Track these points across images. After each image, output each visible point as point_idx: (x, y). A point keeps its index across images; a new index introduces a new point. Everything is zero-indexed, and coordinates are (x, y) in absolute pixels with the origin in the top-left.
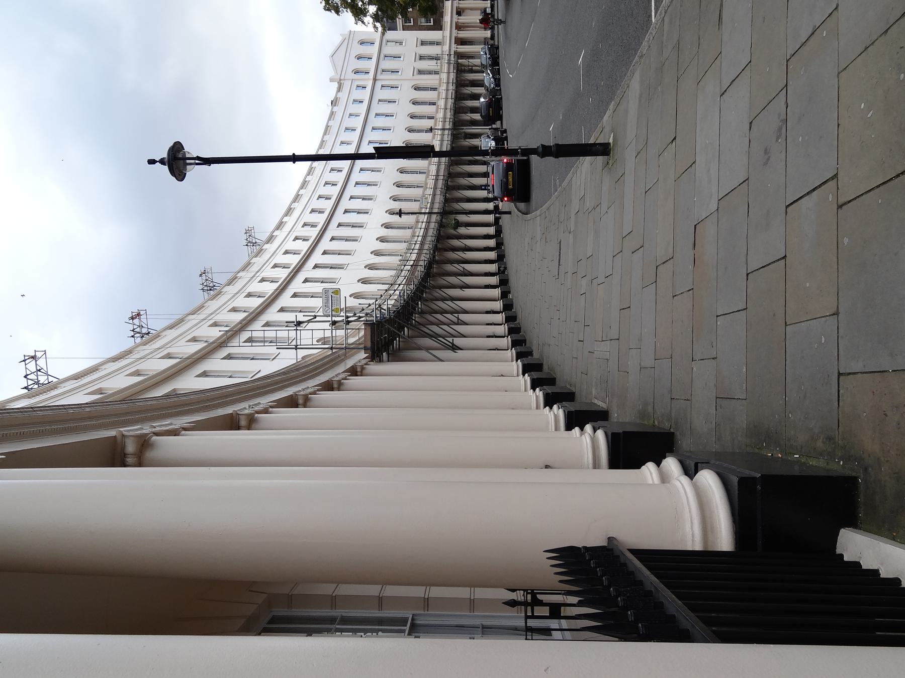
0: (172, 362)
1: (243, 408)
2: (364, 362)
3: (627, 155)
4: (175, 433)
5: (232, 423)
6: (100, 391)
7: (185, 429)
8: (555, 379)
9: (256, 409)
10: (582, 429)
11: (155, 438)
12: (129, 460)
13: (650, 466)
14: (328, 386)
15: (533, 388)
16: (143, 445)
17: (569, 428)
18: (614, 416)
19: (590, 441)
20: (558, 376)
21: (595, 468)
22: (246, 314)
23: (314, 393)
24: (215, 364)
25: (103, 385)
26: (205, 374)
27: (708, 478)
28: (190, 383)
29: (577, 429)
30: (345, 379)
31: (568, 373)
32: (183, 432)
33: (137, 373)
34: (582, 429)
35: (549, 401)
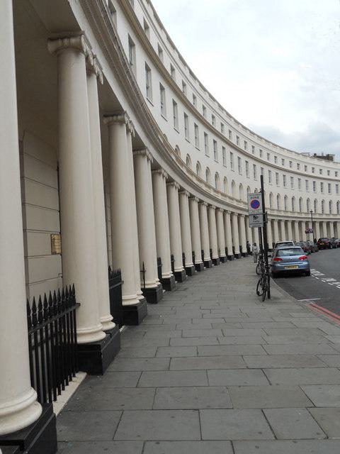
0: (191, 100)
2: (177, 185)
4: (90, 71)
6: (147, 27)
13: (112, 318)
16: (77, 48)
17: (142, 289)
29: (112, 318)
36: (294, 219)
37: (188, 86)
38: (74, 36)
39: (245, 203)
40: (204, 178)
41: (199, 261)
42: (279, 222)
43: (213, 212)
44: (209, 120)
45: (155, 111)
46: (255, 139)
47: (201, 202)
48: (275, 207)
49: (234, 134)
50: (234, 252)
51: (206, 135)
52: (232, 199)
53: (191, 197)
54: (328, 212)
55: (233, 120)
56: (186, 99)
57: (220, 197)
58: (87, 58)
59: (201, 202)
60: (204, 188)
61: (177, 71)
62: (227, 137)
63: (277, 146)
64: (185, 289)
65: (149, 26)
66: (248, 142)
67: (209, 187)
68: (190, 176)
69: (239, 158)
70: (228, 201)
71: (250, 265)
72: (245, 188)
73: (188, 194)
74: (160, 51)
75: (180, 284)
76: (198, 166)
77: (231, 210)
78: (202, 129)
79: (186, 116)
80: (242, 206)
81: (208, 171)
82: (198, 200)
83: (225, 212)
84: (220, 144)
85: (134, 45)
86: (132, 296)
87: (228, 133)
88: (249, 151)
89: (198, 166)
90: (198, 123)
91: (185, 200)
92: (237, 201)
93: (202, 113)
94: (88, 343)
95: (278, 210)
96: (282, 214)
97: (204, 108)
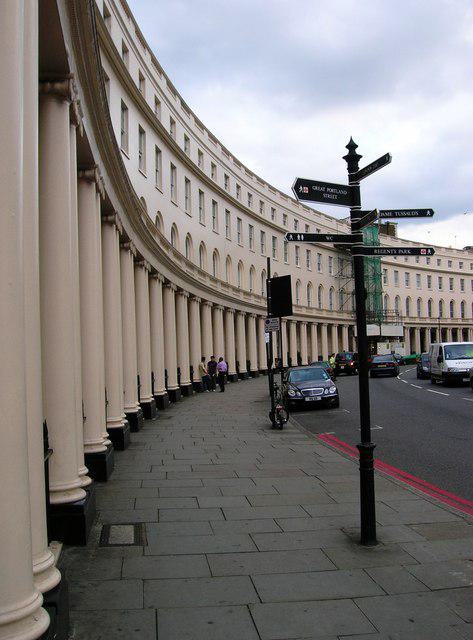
1: (102, 173)
2: (148, 267)
3: (275, 437)
4: (73, 120)
5: (85, 164)
6: (107, 15)
7: (78, 129)
8: (123, 450)
9: (100, 183)
10: (108, 438)
11: (68, 104)
12: (105, 218)
13: (87, 471)
14: (124, 240)
15: (141, 405)
16: (62, 95)
17: (108, 430)
18: (118, 455)
19: (101, 442)
20: (126, 453)
21: (85, 446)
22: (183, 148)
23: (98, 190)
24: (135, 120)
25: (114, 20)
26: (124, 108)
27: (83, 494)
28: (115, 96)
29: (87, 471)
30: (131, 253)
31: (125, 466)
32: (74, 127)
33: (125, 51)
34: (108, 438)
35: (130, 417)
36: (341, 323)
37: (192, 141)
38: (61, 80)
39: (258, 297)
40: (182, 250)
41: (186, 381)
42: (309, 325)
43: (208, 311)
44: (194, 158)
45: (131, 165)
46: (265, 191)
47: (191, 297)
48: (314, 304)
49: (221, 171)
50: (237, 369)
51: (187, 181)
52: (237, 290)
53: (179, 292)
54: (404, 314)
55: (232, 160)
56: (159, 123)
57: (219, 289)
58: (72, 107)
59: (191, 297)
60: (185, 268)
61: (147, 81)
62: (234, 196)
63: (320, 214)
64: (169, 418)
65: (111, 13)
66: (232, 178)
67: (203, 274)
68: (178, 262)
69: (251, 227)
70: (230, 293)
71: (262, 386)
72: (235, 262)
73: (148, 267)
74: (125, 51)
75: (160, 413)
76: (174, 230)
77: (234, 306)
78: (196, 185)
79: (158, 151)
80: (253, 301)
81: (189, 239)
82: (199, 300)
83: (215, 306)
84: (223, 205)
85: (144, 79)
86: (73, 482)
87: (183, 139)
88: (255, 209)
89: (174, 230)
90: (176, 163)
91: (171, 295)
92: (245, 293)
93: (196, 162)
94: (69, 503)
95: (319, 309)
96: (314, 313)
97: (187, 139)
